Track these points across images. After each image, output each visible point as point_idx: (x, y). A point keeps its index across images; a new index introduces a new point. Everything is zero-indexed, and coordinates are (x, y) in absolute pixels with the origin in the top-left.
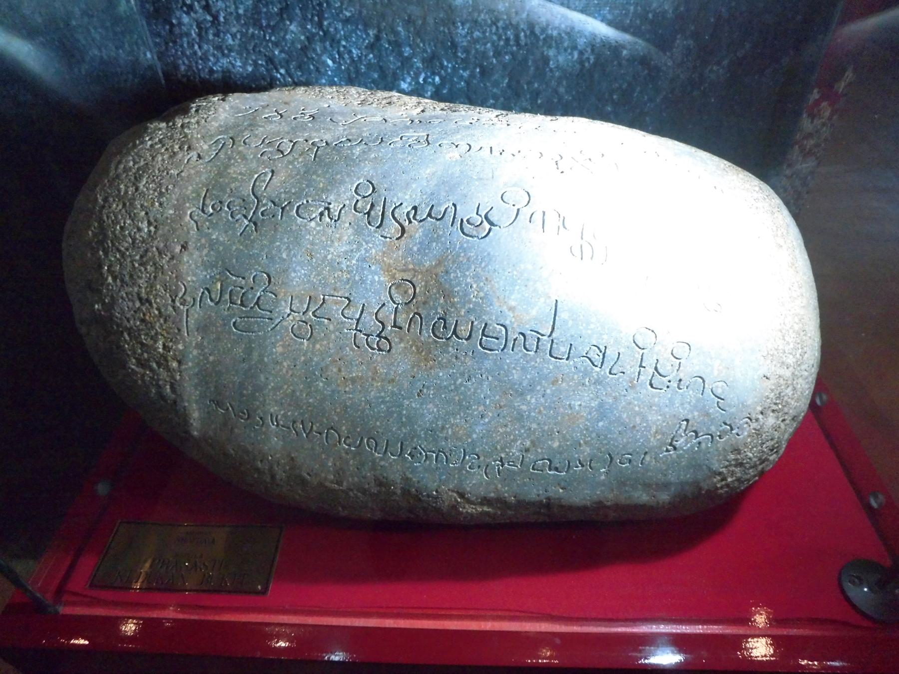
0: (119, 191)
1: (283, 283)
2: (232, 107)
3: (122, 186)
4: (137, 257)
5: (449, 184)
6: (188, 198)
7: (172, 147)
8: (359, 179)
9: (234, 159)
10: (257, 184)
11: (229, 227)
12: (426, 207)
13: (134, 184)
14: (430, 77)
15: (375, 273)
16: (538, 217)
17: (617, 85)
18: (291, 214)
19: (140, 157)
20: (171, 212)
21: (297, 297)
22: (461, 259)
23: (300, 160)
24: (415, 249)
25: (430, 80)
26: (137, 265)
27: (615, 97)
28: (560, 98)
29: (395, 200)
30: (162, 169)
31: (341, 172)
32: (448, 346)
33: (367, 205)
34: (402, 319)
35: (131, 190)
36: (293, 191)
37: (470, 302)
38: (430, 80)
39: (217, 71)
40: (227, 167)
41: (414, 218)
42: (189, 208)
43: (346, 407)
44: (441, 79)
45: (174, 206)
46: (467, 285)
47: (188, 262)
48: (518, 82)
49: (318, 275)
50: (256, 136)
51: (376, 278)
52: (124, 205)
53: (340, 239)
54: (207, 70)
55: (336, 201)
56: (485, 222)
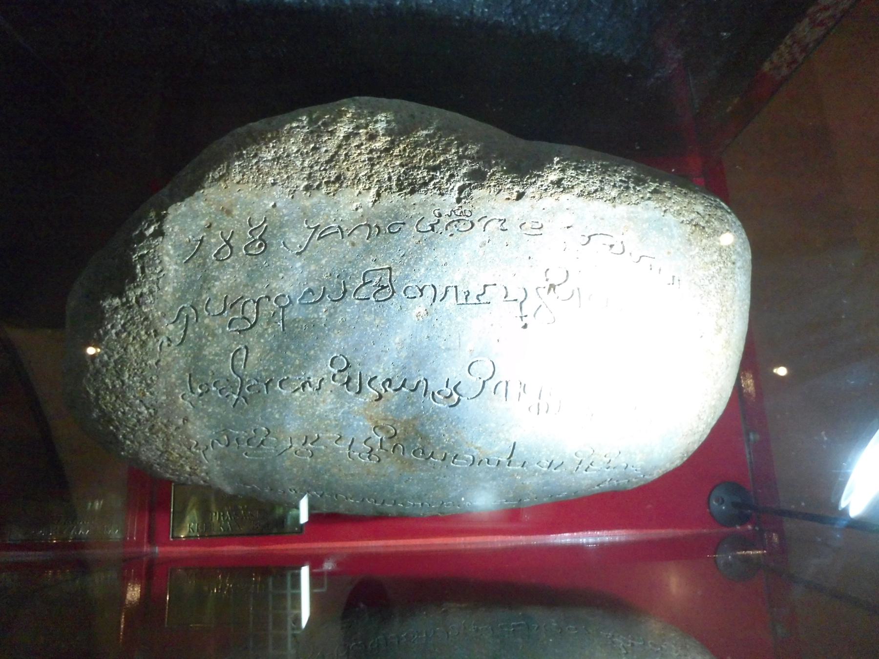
0: (105, 384)
2: (174, 246)
3: (107, 381)
4: (147, 430)
5: (419, 356)
7: (138, 333)
8: (332, 353)
10: (236, 363)
12: (400, 381)
15: (360, 420)
16: (501, 388)
19: (113, 350)
20: (164, 398)
23: (270, 331)
24: (393, 407)
29: (370, 374)
31: (313, 347)
35: (118, 384)
37: (443, 443)
40: (201, 348)
41: (390, 386)
42: (179, 393)
52: (117, 397)
55: (314, 376)
56: (455, 394)
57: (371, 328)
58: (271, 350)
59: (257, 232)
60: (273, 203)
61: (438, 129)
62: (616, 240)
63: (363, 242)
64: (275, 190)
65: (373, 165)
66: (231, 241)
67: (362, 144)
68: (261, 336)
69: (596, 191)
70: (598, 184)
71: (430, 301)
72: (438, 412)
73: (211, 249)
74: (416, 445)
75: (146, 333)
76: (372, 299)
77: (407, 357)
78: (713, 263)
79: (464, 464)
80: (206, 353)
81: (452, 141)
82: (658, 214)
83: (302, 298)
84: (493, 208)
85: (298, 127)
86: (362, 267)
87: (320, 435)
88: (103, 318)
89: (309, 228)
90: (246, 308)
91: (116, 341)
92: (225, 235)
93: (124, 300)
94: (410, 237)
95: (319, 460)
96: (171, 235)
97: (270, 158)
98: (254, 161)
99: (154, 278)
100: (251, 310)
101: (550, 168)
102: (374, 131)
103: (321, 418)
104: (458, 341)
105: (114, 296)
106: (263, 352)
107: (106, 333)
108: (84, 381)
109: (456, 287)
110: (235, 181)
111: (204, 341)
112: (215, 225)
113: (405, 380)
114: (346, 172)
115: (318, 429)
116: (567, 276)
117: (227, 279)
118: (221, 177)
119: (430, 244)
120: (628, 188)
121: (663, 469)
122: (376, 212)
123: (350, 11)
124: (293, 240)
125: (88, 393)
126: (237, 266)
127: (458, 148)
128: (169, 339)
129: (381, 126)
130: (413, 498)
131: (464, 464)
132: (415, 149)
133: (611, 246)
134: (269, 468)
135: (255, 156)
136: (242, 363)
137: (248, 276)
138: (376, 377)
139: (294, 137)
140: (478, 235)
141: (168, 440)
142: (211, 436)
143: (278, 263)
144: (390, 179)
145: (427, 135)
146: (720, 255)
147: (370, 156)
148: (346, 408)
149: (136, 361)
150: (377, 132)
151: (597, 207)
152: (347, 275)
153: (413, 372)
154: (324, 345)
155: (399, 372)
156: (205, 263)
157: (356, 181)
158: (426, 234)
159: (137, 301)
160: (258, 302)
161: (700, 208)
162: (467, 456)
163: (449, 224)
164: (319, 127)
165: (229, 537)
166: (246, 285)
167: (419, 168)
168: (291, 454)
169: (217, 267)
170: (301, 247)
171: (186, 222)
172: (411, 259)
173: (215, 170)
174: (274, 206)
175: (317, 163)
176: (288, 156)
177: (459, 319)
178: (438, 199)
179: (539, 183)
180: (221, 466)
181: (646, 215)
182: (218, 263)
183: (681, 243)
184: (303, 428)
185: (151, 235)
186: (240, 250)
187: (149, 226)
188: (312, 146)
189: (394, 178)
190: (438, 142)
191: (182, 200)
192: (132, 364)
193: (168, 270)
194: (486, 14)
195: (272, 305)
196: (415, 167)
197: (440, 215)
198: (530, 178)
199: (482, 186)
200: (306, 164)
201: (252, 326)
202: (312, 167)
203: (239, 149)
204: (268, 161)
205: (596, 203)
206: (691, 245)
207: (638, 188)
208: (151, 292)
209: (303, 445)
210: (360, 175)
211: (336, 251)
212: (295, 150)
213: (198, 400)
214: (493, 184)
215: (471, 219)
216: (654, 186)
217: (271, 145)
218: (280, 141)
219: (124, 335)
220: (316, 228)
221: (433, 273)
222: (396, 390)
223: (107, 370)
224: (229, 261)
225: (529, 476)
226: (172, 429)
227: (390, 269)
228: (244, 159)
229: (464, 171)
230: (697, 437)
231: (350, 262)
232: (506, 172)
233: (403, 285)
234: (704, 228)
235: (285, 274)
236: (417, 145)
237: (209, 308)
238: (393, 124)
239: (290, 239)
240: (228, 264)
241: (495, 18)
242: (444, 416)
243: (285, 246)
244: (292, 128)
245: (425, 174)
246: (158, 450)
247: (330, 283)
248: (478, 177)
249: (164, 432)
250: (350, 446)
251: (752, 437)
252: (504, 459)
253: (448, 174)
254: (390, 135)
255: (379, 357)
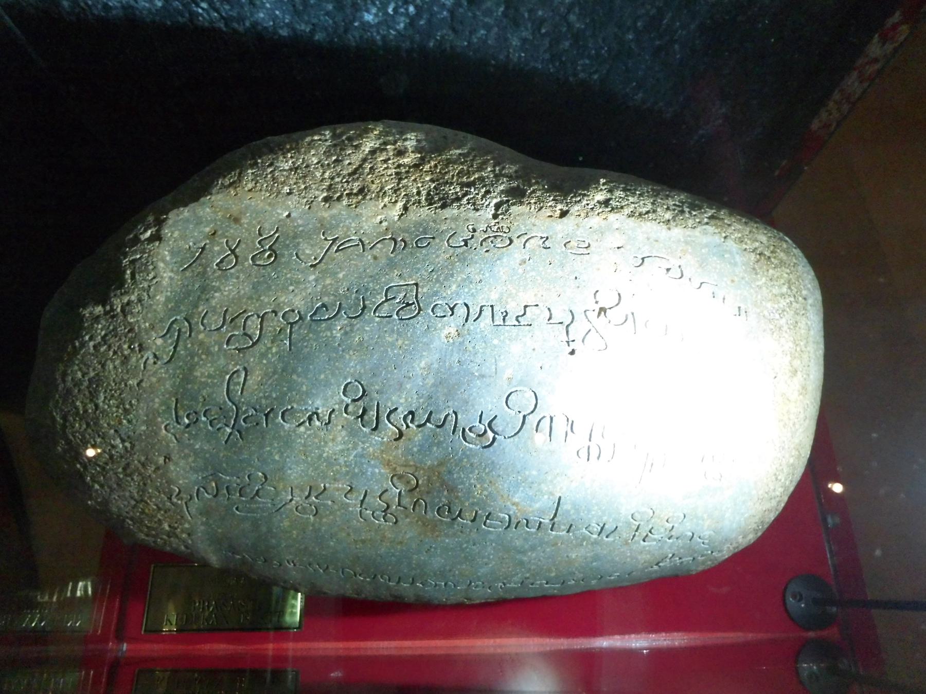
0: (77, 408)
1: (280, 479)
2: (172, 253)
3: (78, 403)
4: (120, 470)
6: (159, 414)
7: (120, 347)
8: (346, 378)
9: (197, 355)
10: (232, 387)
11: (210, 437)
13: (91, 400)
14: (401, 7)
15: (375, 466)
16: (545, 424)
17: (643, 11)
18: (277, 421)
19: (88, 366)
20: (144, 428)
21: (297, 487)
22: (464, 464)
23: (274, 350)
24: (415, 449)
25: (402, 10)
26: (121, 476)
27: (639, 24)
28: (570, 26)
29: (389, 405)
30: (118, 380)
32: (453, 524)
33: (358, 409)
34: (406, 501)
35: (90, 408)
36: (274, 396)
37: (474, 497)
38: (402, 10)
39: (116, 8)
40: (192, 369)
41: (412, 421)
43: (358, 558)
44: (416, 7)
45: (144, 422)
46: (471, 485)
47: (175, 470)
48: (517, 10)
49: (316, 469)
50: (214, 310)
51: (377, 471)
52: (88, 425)
53: (333, 440)
54: (100, 6)
56: (489, 431)
57: (392, 349)
58: (275, 373)
59: (267, 241)
60: (287, 213)
61: (472, 149)
62: (674, 263)
63: (387, 256)
64: (291, 200)
65: (400, 179)
66: (237, 250)
67: (389, 159)
68: (263, 355)
69: (648, 212)
70: (649, 207)
71: (462, 321)
72: (467, 454)
73: (213, 258)
74: (440, 501)
75: (129, 347)
76: (395, 317)
77: (434, 385)
78: (782, 295)
79: (499, 527)
80: (198, 374)
81: (489, 160)
82: (718, 239)
83: (315, 314)
84: (534, 225)
85: (320, 140)
86: (384, 282)
87: (327, 485)
88: (81, 328)
89: (326, 239)
90: (249, 323)
91: (93, 355)
92: (230, 244)
93: (108, 308)
94: (441, 253)
95: (324, 520)
96: (169, 240)
97: (287, 168)
98: (270, 170)
99: (145, 285)
100: (254, 326)
101: (597, 188)
102: (402, 148)
103: (330, 462)
104: (494, 367)
105: (97, 303)
106: (266, 374)
107: (83, 345)
108: (51, 404)
109: (492, 306)
110: (246, 189)
111: (196, 359)
112: (220, 232)
113: (431, 413)
114: (370, 185)
115: (324, 477)
116: (620, 299)
117: (229, 290)
118: (231, 184)
119: (462, 259)
120: (682, 212)
121: (735, 545)
122: (402, 226)
123: (381, 52)
124: (307, 252)
125: (53, 419)
126: (242, 276)
127: (494, 167)
128: (155, 356)
129: (410, 144)
130: (435, 574)
131: (499, 527)
132: (447, 166)
133: (668, 270)
134: (264, 529)
135: (271, 165)
136: (239, 388)
137: (253, 288)
138: (396, 409)
139: (316, 149)
140: (516, 253)
141: (145, 484)
142: (196, 483)
143: (289, 276)
144: (419, 193)
145: (460, 154)
146: (789, 288)
147: (398, 170)
148: (360, 450)
149: (114, 381)
150: (406, 148)
151: (651, 229)
152: (367, 290)
153: (441, 403)
154: (337, 368)
155: (423, 403)
156: (205, 272)
157: (381, 193)
158: (459, 249)
159: (123, 310)
160: (263, 318)
161: (764, 239)
162: (502, 515)
163: (485, 240)
164: (343, 141)
165: (215, 631)
166: (250, 298)
167: (452, 184)
168: (291, 510)
169: (219, 277)
170: (315, 259)
171: (188, 228)
172: (442, 275)
173: (225, 177)
174: (289, 216)
175: (339, 175)
176: (307, 166)
177: (496, 342)
178: (472, 214)
179: (585, 202)
180: (205, 524)
181: (705, 240)
182: (220, 272)
183: (745, 271)
184: (307, 475)
185: (146, 240)
186: (247, 260)
187: (145, 231)
188: (334, 158)
189: (424, 193)
190: (472, 160)
191: (186, 205)
192: (109, 384)
193: (162, 277)
194: (523, 59)
195: (279, 321)
196: (447, 183)
197: (474, 230)
198: (575, 196)
199: (521, 203)
200: (327, 175)
201: (254, 344)
202: (332, 179)
203: (253, 158)
204: (285, 170)
205: (649, 224)
206: (756, 274)
207: (694, 213)
208: (140, 300)
209: (306, 498)
210: (386, 188)
211: (356, 265)
212: (315, 162)
213: (184, 432)
214: (533, 201)
215: (509, 235)
216: (710, 212)
217: (289, 155)
218: (299, 152)
219: (103, 349)
220: (334, 240)
221: (466, 290)
222: (419, 426)
223: (79, 391)
224: (232, 271)
225: (576, 546)
226: (151, 469)
227: (416, 284)
228: (258, 167)
229: (502, 188)
230: (774, 503)
231: (371, 277)
232: (547, 191)
233: (431, 303)
234: (769, 258)
235: (296, 288)
236: (449, 162)
237: (205, 321)
238: (424, 143)
239: (303, 250)
240: (232, 274)
241: (532, 64)
242: (475, 460)
243: (298, 257)
244: (313, 140)
245: (458, 190)
246: (132, 498)
247: (347, 298)
248: (517, 195)
249: (140, 474)
250: (362, 501)
251: (830, 520)
252: (546, 521)
253: (483, 190)
254: (420, 153)
255: (401, 385)
